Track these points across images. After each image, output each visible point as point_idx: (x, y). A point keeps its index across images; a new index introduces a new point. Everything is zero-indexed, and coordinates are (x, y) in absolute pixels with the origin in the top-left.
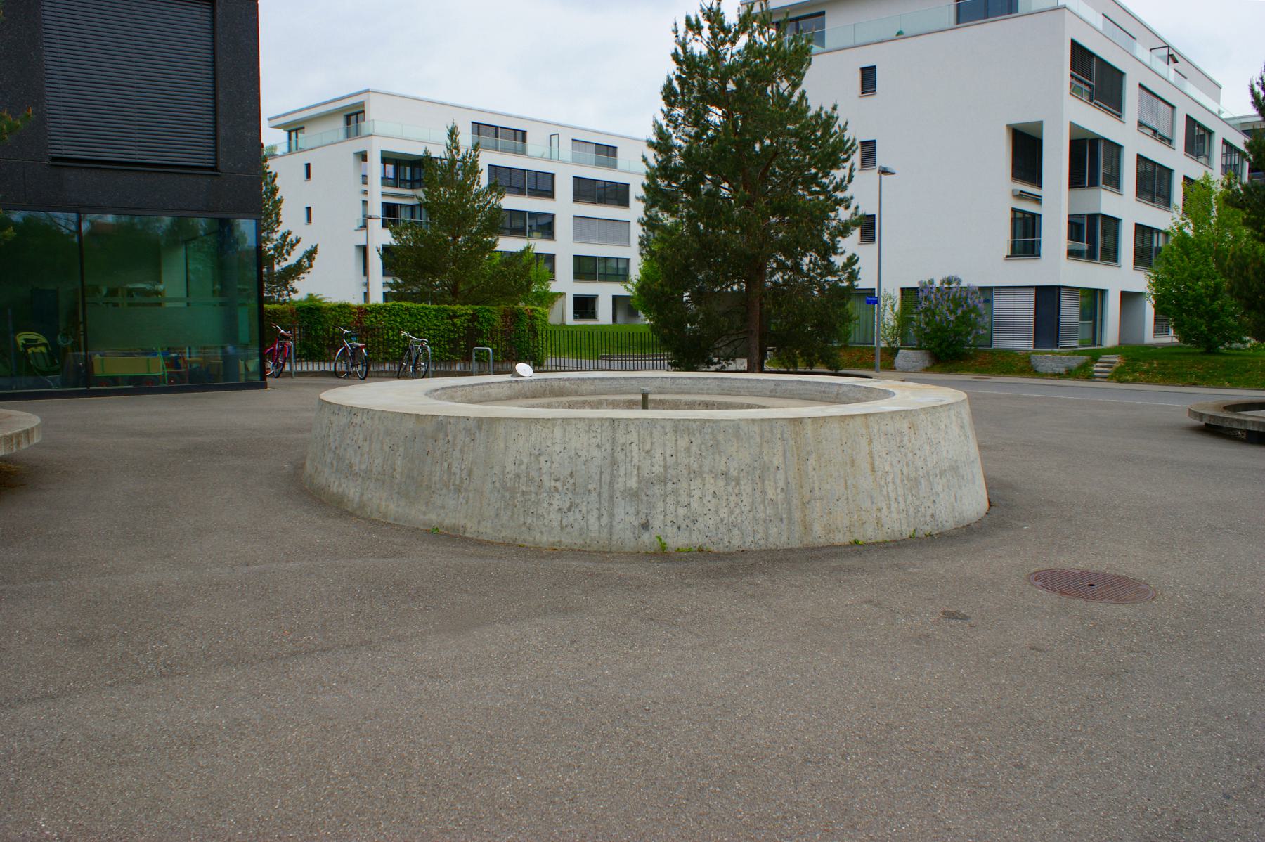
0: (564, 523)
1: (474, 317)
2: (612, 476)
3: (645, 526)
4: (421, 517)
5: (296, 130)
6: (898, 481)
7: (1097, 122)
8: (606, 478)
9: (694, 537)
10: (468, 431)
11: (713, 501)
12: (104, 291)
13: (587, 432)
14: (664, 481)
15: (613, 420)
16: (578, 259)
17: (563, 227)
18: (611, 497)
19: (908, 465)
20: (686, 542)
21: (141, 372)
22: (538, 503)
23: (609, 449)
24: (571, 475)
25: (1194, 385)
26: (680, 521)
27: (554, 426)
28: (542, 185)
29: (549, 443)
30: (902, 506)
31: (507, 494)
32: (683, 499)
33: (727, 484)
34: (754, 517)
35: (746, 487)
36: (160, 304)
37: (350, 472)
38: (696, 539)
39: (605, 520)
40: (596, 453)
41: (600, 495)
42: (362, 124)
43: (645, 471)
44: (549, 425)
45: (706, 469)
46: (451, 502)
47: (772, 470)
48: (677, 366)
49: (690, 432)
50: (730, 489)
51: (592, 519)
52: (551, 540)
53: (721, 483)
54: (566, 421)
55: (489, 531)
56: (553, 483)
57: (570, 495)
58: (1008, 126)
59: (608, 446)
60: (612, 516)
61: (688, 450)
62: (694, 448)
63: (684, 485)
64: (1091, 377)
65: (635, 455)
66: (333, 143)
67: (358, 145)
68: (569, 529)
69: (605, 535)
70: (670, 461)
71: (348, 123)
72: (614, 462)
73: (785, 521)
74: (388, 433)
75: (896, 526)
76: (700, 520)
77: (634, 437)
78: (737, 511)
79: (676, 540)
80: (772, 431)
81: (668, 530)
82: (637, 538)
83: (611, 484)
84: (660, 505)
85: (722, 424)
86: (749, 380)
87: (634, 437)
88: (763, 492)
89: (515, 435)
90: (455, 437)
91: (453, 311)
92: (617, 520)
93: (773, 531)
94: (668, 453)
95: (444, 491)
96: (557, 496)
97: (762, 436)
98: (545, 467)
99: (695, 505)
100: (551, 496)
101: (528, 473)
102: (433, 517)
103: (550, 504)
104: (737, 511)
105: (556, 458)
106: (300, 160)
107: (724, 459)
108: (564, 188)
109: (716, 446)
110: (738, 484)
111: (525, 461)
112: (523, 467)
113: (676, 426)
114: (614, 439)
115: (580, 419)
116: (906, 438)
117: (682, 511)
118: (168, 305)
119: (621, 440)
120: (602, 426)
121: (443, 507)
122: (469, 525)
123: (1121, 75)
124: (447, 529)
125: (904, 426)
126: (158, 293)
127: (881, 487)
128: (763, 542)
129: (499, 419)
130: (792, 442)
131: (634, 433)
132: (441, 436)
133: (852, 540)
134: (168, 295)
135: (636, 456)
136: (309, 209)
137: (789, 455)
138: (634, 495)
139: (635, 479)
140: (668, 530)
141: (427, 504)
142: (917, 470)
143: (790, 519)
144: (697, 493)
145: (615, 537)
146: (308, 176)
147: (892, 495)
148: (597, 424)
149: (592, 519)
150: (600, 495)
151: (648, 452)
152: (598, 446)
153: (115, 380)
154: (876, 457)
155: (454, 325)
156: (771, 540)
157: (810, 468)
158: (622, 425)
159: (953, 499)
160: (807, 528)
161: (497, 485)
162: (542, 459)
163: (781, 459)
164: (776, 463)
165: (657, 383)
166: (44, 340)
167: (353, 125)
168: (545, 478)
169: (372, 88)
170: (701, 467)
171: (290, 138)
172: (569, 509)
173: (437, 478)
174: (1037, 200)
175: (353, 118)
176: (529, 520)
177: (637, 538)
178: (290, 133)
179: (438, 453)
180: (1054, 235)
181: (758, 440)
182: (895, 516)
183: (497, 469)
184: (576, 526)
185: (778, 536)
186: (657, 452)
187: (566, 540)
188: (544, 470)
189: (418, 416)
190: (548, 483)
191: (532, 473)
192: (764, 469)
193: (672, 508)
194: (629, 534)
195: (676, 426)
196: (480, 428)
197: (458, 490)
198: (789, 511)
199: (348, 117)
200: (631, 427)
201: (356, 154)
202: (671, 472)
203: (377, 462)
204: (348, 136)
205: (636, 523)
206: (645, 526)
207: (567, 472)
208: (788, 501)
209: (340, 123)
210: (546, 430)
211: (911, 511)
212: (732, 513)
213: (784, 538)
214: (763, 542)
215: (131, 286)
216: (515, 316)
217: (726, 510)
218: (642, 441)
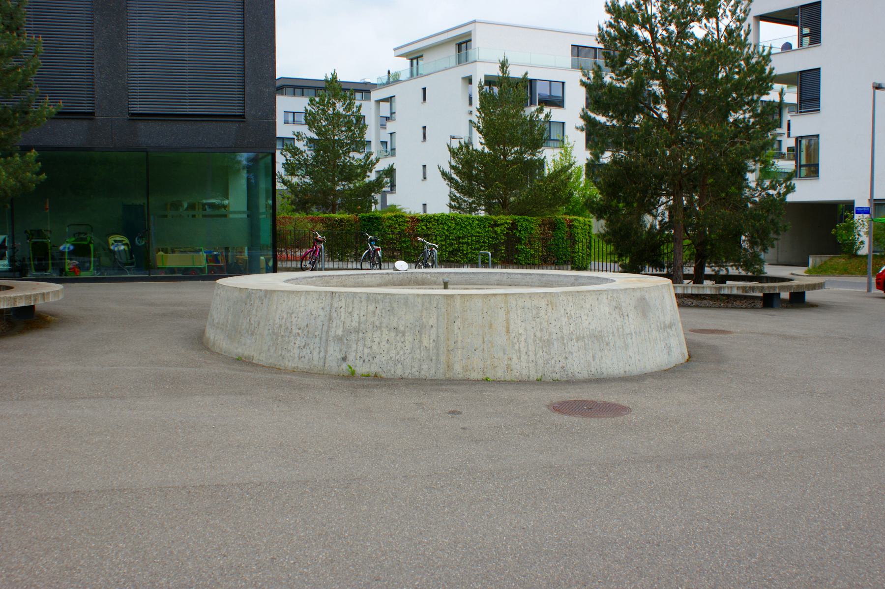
1: (514, 225)
2: (329, 327)
3: (344, 359)
5: (417, 58)
6: (530, 341)
8: (325, 328)
9: (372, 367)
10: (260, 298)
11: (387, 345)
12: (185, 205)
14: (357, 331)
19: (541, 330)
20: (367, 370)
21: (189, 265)
22: (288, 343)
24: (307, 326)
26: (365, 357)
30: (532, 357)
32: (368, 343)
33: (397, 335)
34: (413, 358)
35: (409, 338)
36: (225, 216)
38: (373, 369)
40: (321, 313)
41: (321, 338)
42: (469, 51)
43: (347, 325)
45: (384, 325)
46: (249, 341)
47: (428, 327)
48: (626, 269)
49: (376, 301)
50: (398, 338)
51: (316, 355)
53: (393, 334)
54: (308, 292)
59: (328, 309)
60: (326, 351)
61: (374, 313)
62: (378, 312)
63: (369, 334)
65: (343, 314)
66: (446, 69)
67: (466, 70)
69: (321, 364)
70: (363, 319)
71: (459, 50)
72: (330, 319)
73: (434, 361)
75: (525, 372)
77: (343, 303)
78: (401, 353)
79: (362, 369)
80: (430, 302)
81: (357, 362)
83: (328, 332)
84: (354, 346)
85: (397, 297)
86: (559, 276)
87: (343, 303)
88: (421, 342)
91: (495, 221)
92: (329, 354)
93: (425, 367)
94: (362, 314)
96: (299, 338)
97: (423, 305)
98: (294, 320)
99: (375, 347)
100: (296, 339)
102: (240, 350)
104: (401, 353)
105: (300, 315)
106: (420, 83)
107: (396, 319)
109: (391, 311)
110: (404, 335)
113: (368, 297)
114: (331, 305)
116: (542, 313)
117: (366, 351)
118: (231, 216)
119: (335, 305)
125: (543, 303)
126: (225, 207)
127: (513, 345)
128: (417, 373)
129: (275, 291)
130: (443, 310)
131: (343, 301)
133: (484, 377)
134: (231, 209)
136: (424, 128)
137: (440, 318)
138: (339, 339)
139: (341, 329)
140: (357, 362)
142: (550, 334)
143: (438, 360)
144: (377, 340)
146: (424, 99)
147: (523, 350)
148: (323, 294)
150: (321, 338)
151: (350, 313)
153: (172, 270)
154: (512, 322)
155: (496, 232)
156: (423, 372)
157: (456, 328)
159: (590, 358)
160: (449, 367)
162: (293, 316)
163: (435, 321)
164: (431, 323)
165: (497, 277)
166: (127, 241)
167: (463, 52)
168: (294, 327)
169: (478, 18)
170: (381, 323)
171: (412, 65)
175: (464, 46)
178: (412, 60)
181: (420, 308)
182: (524, 364)
183: (271, 322)
184: (307, 358)
185: (428, 371)
187: (301, 366)
190: (295, 331)
191: (288, 325)
192: (423, 327)
193: (360, 348)
194: (334, 364)
195: (368, 297)
197: (252, 334)
198: (438, 355)
199: (459, 46)
200: (342, 298)
201: (463, 78)
202: (363, 326)
204: (459, 62)
206: (344, 359)
207: (305, 324)
208: (437, 348)
209: (452, 50)
211: (541, 362)
212: (398, 353)
213: (432, 372)
214: (417, 373)
215: (204, 201)
216: (554, 226)
217: (394, 352)
218: (347, 306)
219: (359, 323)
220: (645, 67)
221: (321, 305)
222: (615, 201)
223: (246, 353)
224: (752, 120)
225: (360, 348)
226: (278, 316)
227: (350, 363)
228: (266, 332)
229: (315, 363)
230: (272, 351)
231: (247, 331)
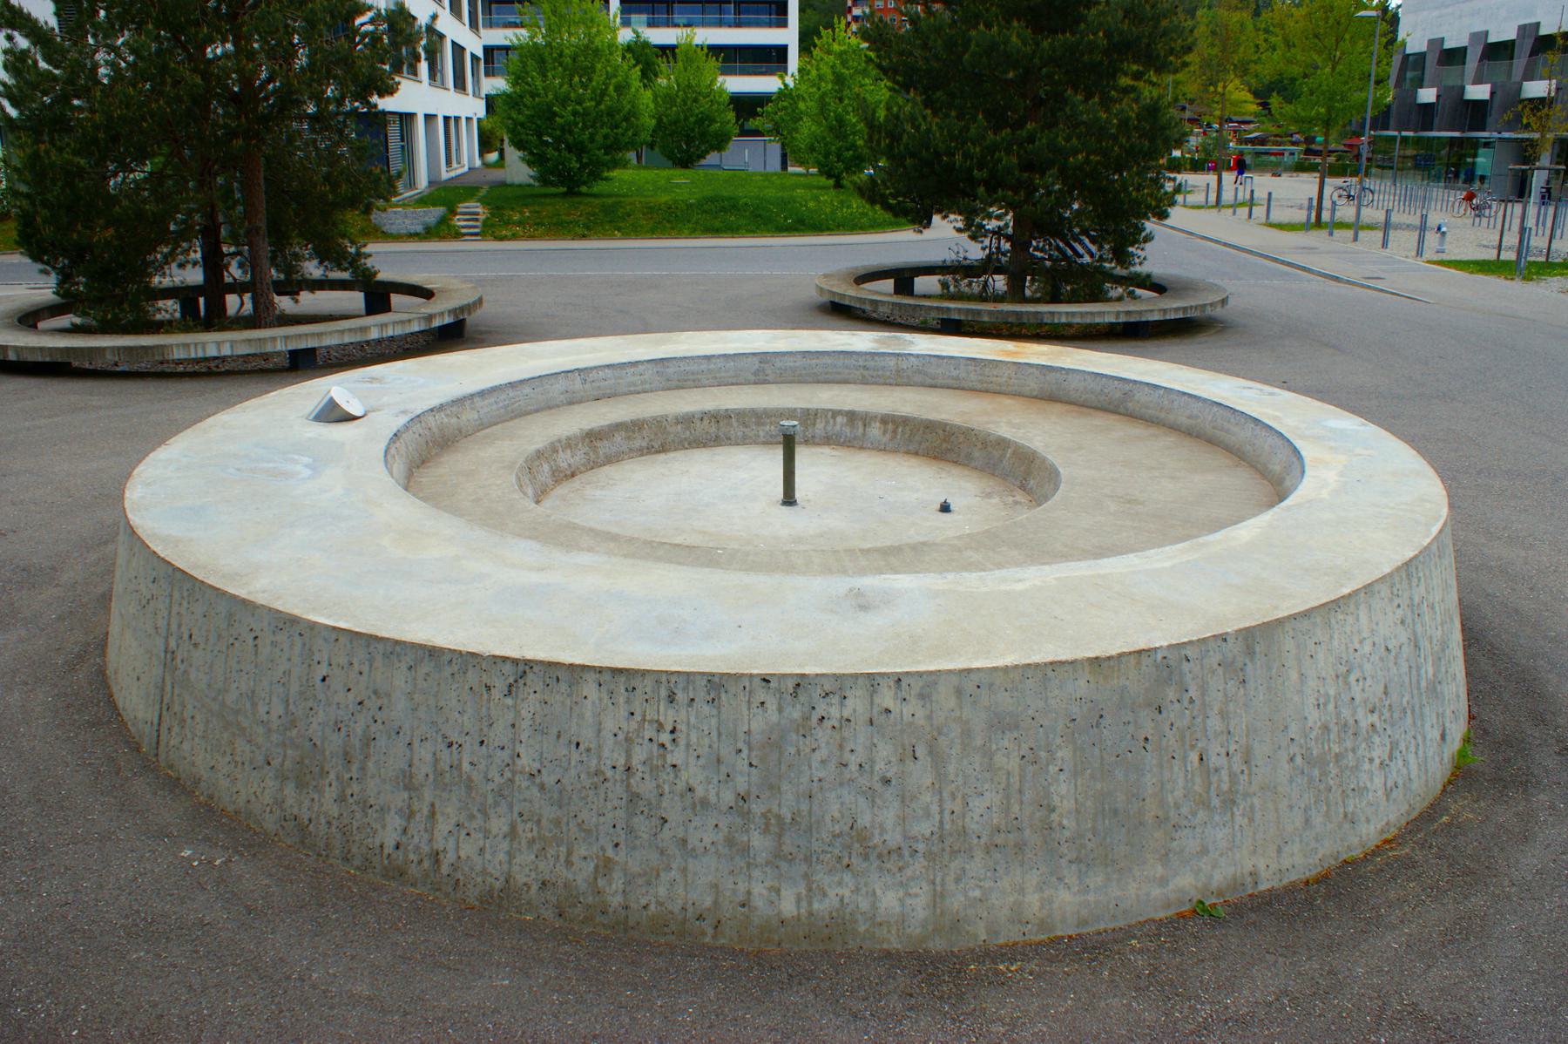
4: (1156, 892)
25: (584, 237)
37: (858, 847)
55: (1298, 860)
64: (457, 235)
74: (1002, 724)
90: (1204, 690)
95: (1201, 814)
98: (1356, 690)
101: (1338, 715)
102: (1186, 883)
111: (1332, 693)
121: (1204, 851)
122: (1262, 866)
124: (1220, 893)
129: (1280, 622)
132: (1171, 694)
141: (1164, 858)
161: (1298, 760)
162: (1352, 678)
168: (1361, 714)
173: (1179, 793)
179: (1171, 739)
183: (1294, 730)
189: (1096, 662)
190: (1365, 720)
196: (1250, 652)
197: (1229, 802)
203: (978, 805)
210: (1350, 619)
222: (413, 96)
223: (1220, 875)
224: (229, 46)
228: (1285, 769)
230: (1318, 820)
231: (1206, 805)
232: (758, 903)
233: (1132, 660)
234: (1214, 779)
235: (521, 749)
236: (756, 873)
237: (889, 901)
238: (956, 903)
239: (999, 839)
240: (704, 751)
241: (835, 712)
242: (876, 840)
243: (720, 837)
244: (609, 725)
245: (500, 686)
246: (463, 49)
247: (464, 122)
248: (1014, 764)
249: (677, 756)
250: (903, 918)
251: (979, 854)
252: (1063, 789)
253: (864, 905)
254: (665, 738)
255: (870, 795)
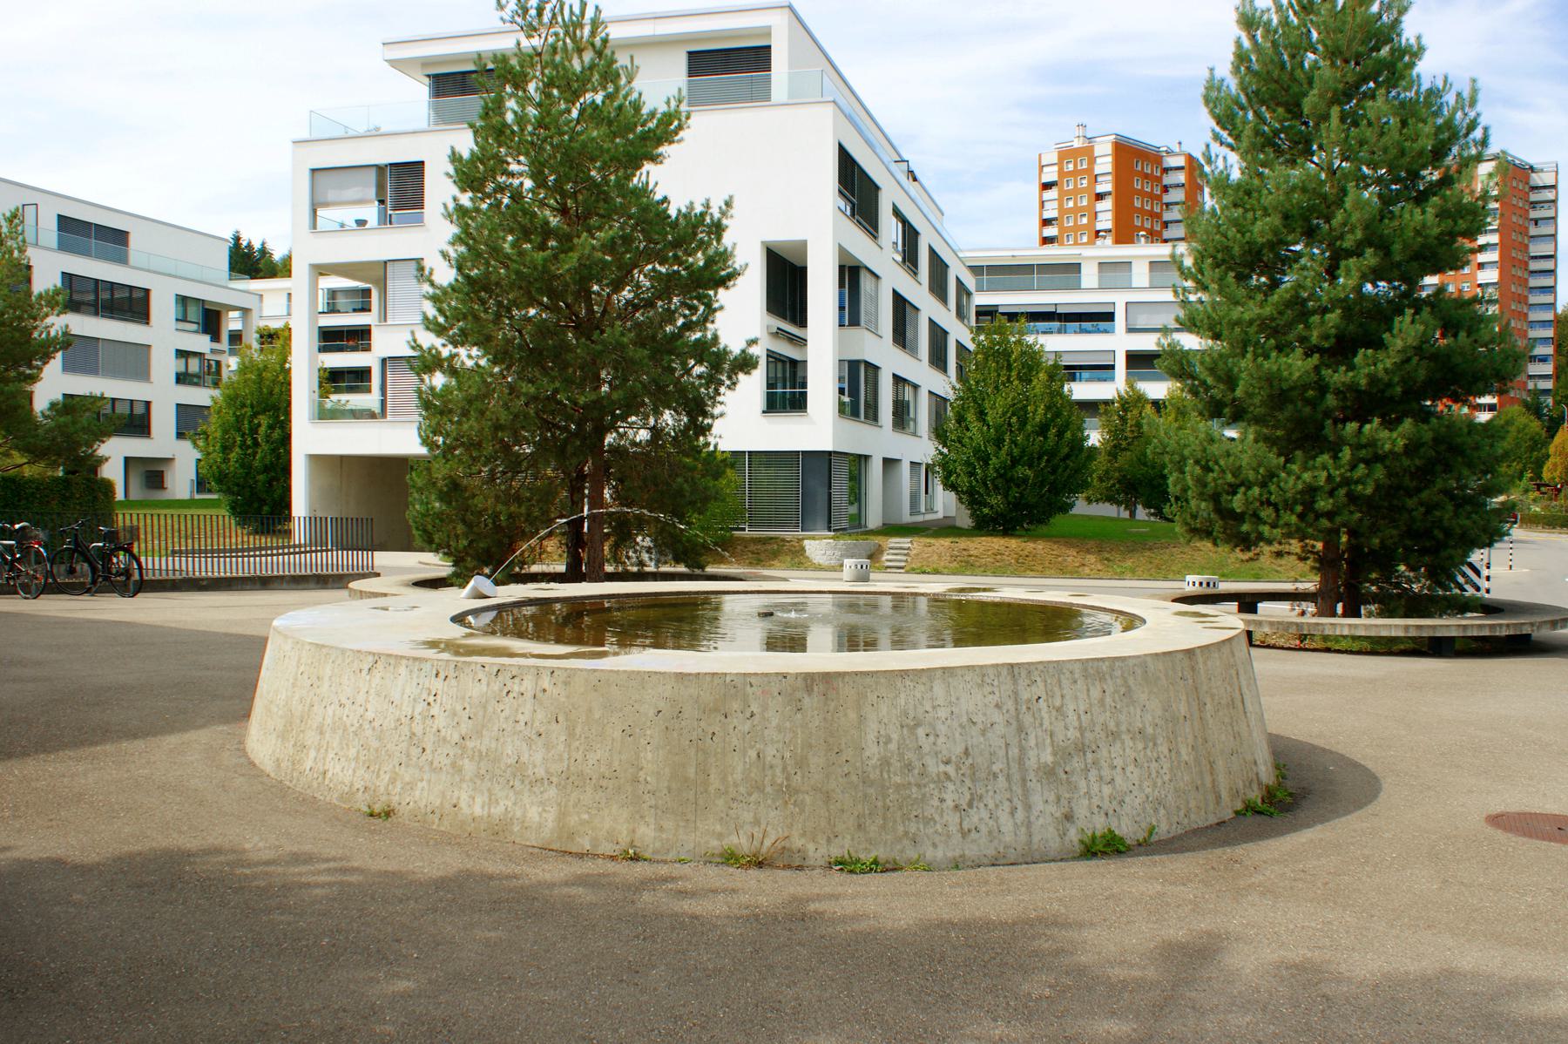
0: (966, 826)
2: (1022, 749)
3: (1069, 817)
4: (715, 843)
7: (861, 247)
8: (1014, 752)
13: (981, 686)
14: (1081, 749)
15: (1012, 665)
16: (182, 409)
17: (164, 366)
18: (1024, 780)
23: (1012, 709)
24: (966, 752)
26: (1106, 805)
27: (931, 680)
28: (134, 305)
29: (928, 708)
31: (871, 791)
39: (1020, 815)
40: (997, 717)
41: (1008, 778)
43: (1060, 737)
44: (924, 679)
45: (1123, 728)
51: (1004, 817)
52: (950, 854)
56: (942, 768)
57: (968, 783)
58: (804, 243)
59: (1010, 705)
60: (1028, 807)
61: (1102, 702)
62: (1108, 700)
63: (1104, 752)
68: (974, 835)
72: (1021, 729)
76: (1127, 800)
82: (1063, 835)
83: (1021, 761)
84: (1082, 784)
85: (1131, 663)
87: (1039, 690)
89: (872, 697)
94: (1082, 708)
96: (951, 787)
98: (927, 744)
101: (901, 755)
103: (942, 800)
105: (942, 729)
108: (163, 307)
111: (895, 736)
112: (893, 746)
113: (1086, 670)
114: (1016, 693)
115: (968, 667)
117: (1107, 790)
119: (1025, 695)
120: (999, 675)
122: (811, 847)
123: (877, 188)
131: (1040, 684)
135: (1046, 716)
138: (1049, 773)
139: (1049, 750)
144: (1119, 762)
145: (1036, 839)
148: (991, 672)
149: (1004, 817)
152: (997, 706)
158: (1024, 673)
161: (854, 778)
162: (921, 732)
170: (1118, 725)
172: (970, 805)
174: (801, 342)
176: (913, 828)
177: (1063, 835)
180: (822, 385)
183: (848, 754)
184: (984, 830)
186: (1070, 707)
188: (926, 748)
190: (934, 768)
191: (909, 755)
195: (1086, 670)
202: (1088, 734)
205: (1058, 814)
206: (1069, 817)
207: (959, 749)
219: (1081, 729)
220: (598, 378)
221: (993, 699)
225: (1095, 788)
226: (871, 737)
227: (1081, 823)
229: (1008, 838)
232: (463, 804)
233: (708, 678)
234: (769, 773)
235: (369, 706)
236: (464, 786)
237: (533, 813)
238: (573, 820)
239: (604, 783)
240: (448, 707)
241: (516, 688)
242: (530, 772)
243: (448, 762)
244: (408, 691)
245: (366, 667)
246: (946, 333)
247: (875, 470)
248: (617, 734)
249: (435, 710)
250: (540, 826)
251: (589, 789)
252: (649, 756)
253: (519, 814)
254: (431, 699)
255: (529, 741)
